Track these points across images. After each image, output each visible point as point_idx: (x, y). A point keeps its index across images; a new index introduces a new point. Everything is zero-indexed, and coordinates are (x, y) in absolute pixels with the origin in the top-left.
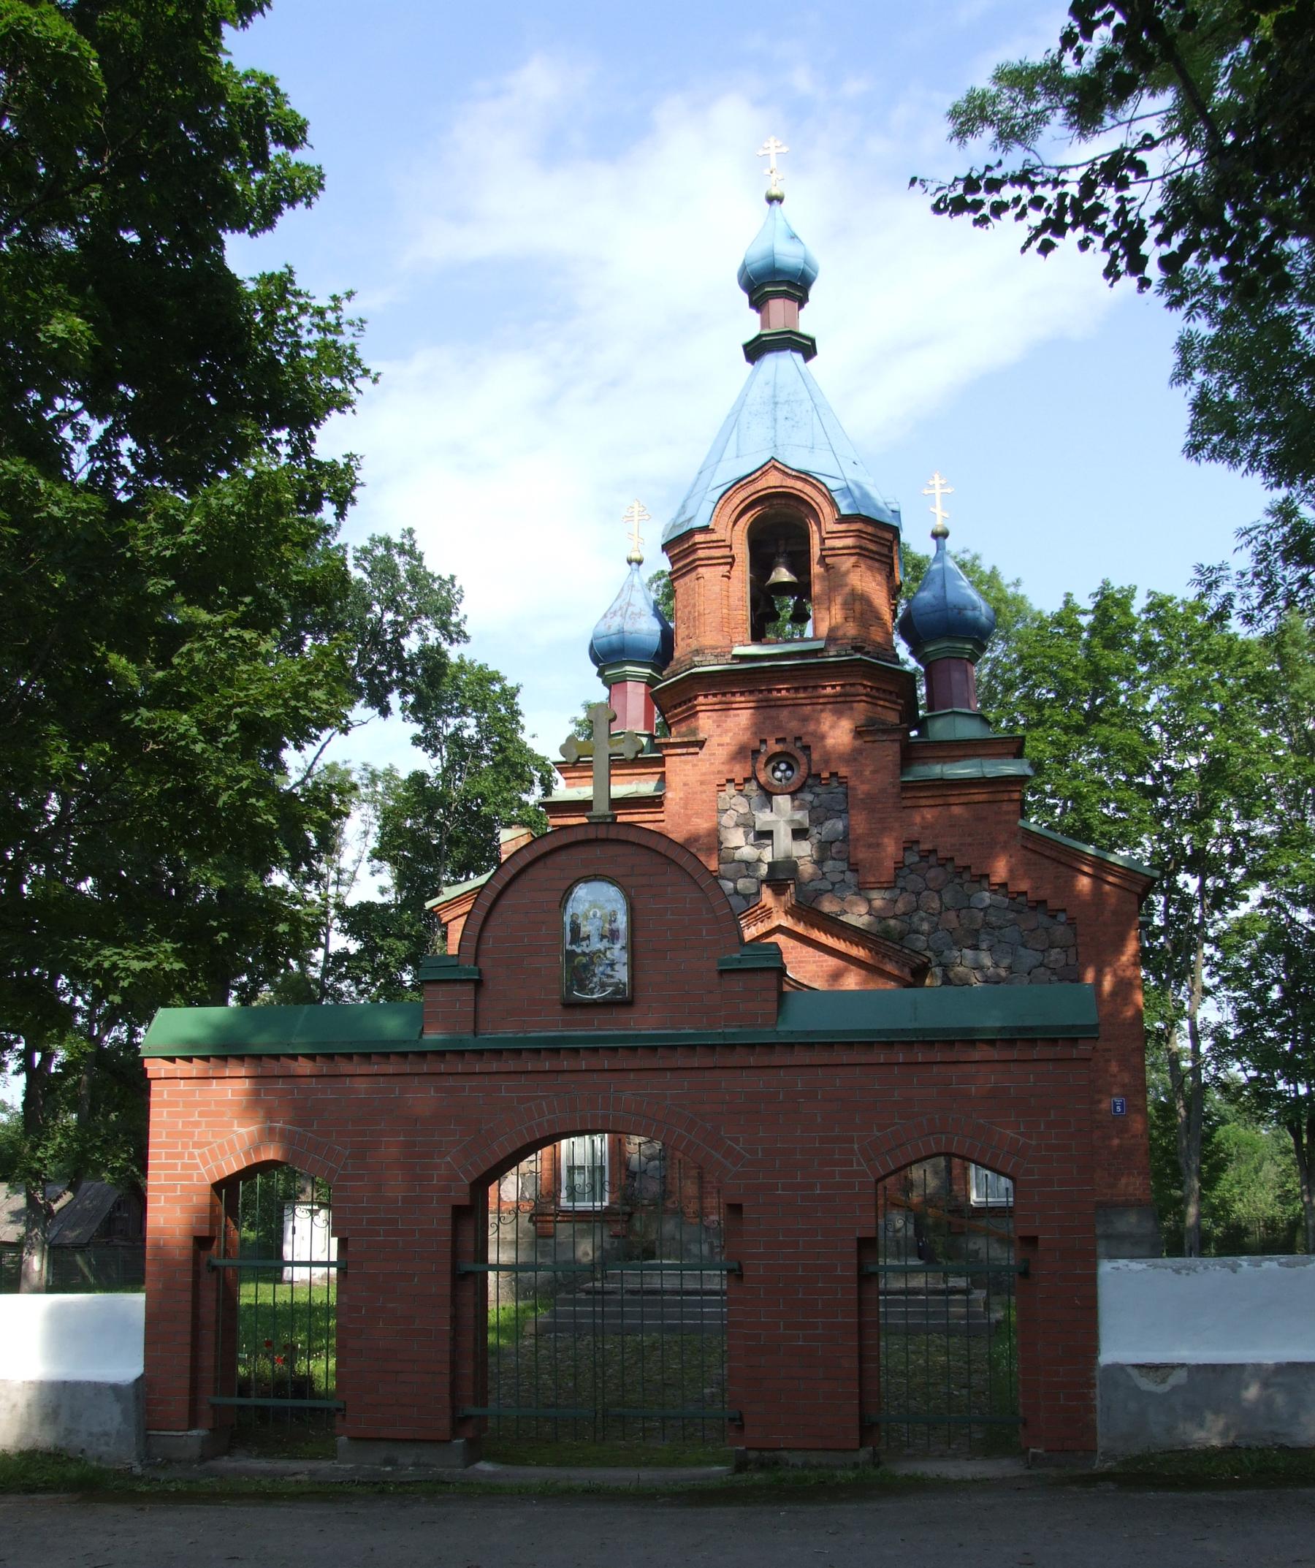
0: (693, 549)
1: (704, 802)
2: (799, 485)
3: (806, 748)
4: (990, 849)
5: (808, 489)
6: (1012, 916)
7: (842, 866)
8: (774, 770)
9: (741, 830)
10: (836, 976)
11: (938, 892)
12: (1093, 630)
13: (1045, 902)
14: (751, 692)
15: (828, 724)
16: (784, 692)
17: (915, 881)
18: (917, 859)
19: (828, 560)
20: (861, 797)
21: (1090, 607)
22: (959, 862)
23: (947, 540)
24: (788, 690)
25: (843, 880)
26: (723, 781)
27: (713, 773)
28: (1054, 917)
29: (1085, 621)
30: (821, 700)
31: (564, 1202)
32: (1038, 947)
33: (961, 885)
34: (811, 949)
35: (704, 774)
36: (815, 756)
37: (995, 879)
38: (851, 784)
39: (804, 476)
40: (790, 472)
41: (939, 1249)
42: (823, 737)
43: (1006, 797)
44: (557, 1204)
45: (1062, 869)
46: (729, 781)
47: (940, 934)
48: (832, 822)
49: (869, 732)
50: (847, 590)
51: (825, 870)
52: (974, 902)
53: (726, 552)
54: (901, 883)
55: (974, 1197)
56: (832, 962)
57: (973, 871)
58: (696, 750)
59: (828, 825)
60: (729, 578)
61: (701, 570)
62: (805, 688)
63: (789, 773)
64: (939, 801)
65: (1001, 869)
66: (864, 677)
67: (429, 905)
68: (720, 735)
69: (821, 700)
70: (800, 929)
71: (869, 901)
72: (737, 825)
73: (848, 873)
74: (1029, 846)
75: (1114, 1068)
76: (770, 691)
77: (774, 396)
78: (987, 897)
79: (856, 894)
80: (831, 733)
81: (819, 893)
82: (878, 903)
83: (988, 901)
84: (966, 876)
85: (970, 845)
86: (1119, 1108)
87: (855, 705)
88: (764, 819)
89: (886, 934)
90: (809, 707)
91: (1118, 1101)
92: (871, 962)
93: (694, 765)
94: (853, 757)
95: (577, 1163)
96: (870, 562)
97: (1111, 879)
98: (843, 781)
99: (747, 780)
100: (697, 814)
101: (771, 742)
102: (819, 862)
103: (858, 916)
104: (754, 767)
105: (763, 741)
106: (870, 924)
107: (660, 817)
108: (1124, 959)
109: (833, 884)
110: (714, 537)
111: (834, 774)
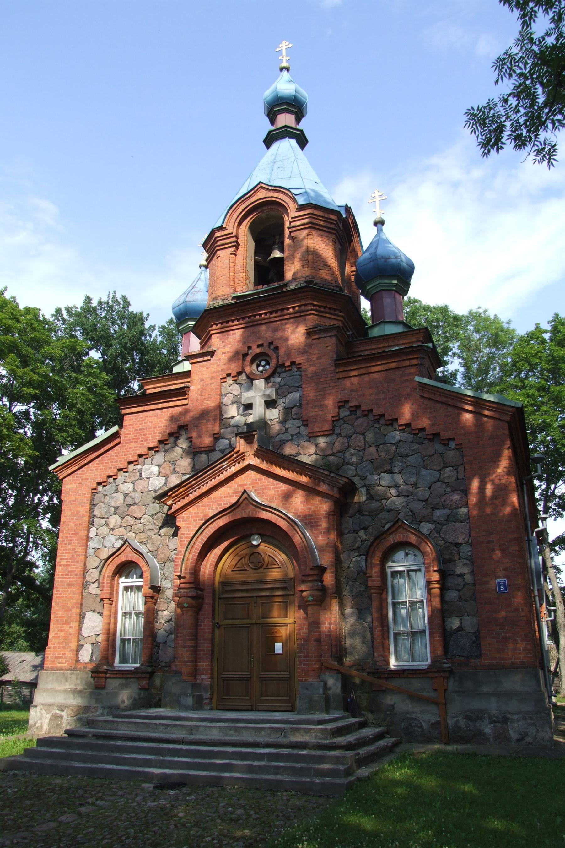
0: (215, 241)
1: (212, 390)
2: (276, 194)
3: (277, 348)
4: (397, 401)
5: (281, 196)
6: (416, 447)
7: (298, 423)
8: (258, 366)
9: (235, 406)
10: (287, 497)
11: (363, 434)
12: (551, 340)
13: (438, 434)
14: (244, 318)
15: (290, 331)
16: (263, 316)
17: (347, 429)
18: (348, 413)
19: (293, 234)
20: (311, 375)
21: (549, 328)
22: (376, 412)
23: (384, 227)
24: (265, 314)
25: (299, 433)
26: (225, 376)
27: (219, 371)
28: (446, 445)
29: (547, 336)
30: (286, 317)
31: (117, 663)
32: (435, 468)
33: (379, 428)
34: (271, 480)
35: (214, 372)
36: (282, 351)
37: (402, 421)
38: (304, 367)
39: (278, 189)
40: (270, 188)
41: (364, 704)
42: (287, 339)
43: (407, 363)
44: (112, 665)
45: (450, 409)
46: (229, 375)
47: (364, 464)
48: (292, 394)
49: (315, 333)
50: (303, 249)
51: (287, 426)
52: (389, 439)
53: (234, 239)
54: (337, 431)
55: (393, 663)
56: (284, 487)
57: (387, 417)
58: (209, 358)
59: (291, 396)
60: (236, 255)
61: (218, 252)
62: (276, 312)
63: (268, 367)
64: (363, 371)
65: (406, 412)
66: (313, 299)
67: (50, 468)
68: (224, 348)
69: (286, 317)
70: (264, 466)
71: (316, 445)
72: (233, 403)
73: (302, 428)
74: (425, 395)
75: (497, 554)
76: (255, 316)
77: (275, 159)
78: (397, 435)
79: (307, 441)
80: (292, 337)
81: (283, 443)
82: (322, 445)
83: (398, 438)
84: (382, 422)
85: (384, 399)
86: (502, 588)
87: (308, 317)
88: (247, 396)
89: (328, 467)
90: (278, 323)
91: (502, 581)
92: (311, 485)
93: (208, 368)
94: (305, 350)
95: (127, 636)
96: (321, 232)
97: (486, 413)
98: (299, 366)
99: (239, 373)
100: (208, 398)
101: (254, 347)
102: (283, 422)
103: (308, 455)
104: (243, 364)
105: (250, 348)
106: (316, 460)
107: (185, 402)
108: (499, 471)
109: (292, 436)
110: (226, 232)
111: (293, 363)
